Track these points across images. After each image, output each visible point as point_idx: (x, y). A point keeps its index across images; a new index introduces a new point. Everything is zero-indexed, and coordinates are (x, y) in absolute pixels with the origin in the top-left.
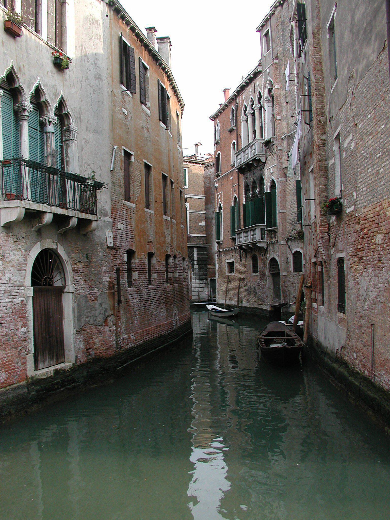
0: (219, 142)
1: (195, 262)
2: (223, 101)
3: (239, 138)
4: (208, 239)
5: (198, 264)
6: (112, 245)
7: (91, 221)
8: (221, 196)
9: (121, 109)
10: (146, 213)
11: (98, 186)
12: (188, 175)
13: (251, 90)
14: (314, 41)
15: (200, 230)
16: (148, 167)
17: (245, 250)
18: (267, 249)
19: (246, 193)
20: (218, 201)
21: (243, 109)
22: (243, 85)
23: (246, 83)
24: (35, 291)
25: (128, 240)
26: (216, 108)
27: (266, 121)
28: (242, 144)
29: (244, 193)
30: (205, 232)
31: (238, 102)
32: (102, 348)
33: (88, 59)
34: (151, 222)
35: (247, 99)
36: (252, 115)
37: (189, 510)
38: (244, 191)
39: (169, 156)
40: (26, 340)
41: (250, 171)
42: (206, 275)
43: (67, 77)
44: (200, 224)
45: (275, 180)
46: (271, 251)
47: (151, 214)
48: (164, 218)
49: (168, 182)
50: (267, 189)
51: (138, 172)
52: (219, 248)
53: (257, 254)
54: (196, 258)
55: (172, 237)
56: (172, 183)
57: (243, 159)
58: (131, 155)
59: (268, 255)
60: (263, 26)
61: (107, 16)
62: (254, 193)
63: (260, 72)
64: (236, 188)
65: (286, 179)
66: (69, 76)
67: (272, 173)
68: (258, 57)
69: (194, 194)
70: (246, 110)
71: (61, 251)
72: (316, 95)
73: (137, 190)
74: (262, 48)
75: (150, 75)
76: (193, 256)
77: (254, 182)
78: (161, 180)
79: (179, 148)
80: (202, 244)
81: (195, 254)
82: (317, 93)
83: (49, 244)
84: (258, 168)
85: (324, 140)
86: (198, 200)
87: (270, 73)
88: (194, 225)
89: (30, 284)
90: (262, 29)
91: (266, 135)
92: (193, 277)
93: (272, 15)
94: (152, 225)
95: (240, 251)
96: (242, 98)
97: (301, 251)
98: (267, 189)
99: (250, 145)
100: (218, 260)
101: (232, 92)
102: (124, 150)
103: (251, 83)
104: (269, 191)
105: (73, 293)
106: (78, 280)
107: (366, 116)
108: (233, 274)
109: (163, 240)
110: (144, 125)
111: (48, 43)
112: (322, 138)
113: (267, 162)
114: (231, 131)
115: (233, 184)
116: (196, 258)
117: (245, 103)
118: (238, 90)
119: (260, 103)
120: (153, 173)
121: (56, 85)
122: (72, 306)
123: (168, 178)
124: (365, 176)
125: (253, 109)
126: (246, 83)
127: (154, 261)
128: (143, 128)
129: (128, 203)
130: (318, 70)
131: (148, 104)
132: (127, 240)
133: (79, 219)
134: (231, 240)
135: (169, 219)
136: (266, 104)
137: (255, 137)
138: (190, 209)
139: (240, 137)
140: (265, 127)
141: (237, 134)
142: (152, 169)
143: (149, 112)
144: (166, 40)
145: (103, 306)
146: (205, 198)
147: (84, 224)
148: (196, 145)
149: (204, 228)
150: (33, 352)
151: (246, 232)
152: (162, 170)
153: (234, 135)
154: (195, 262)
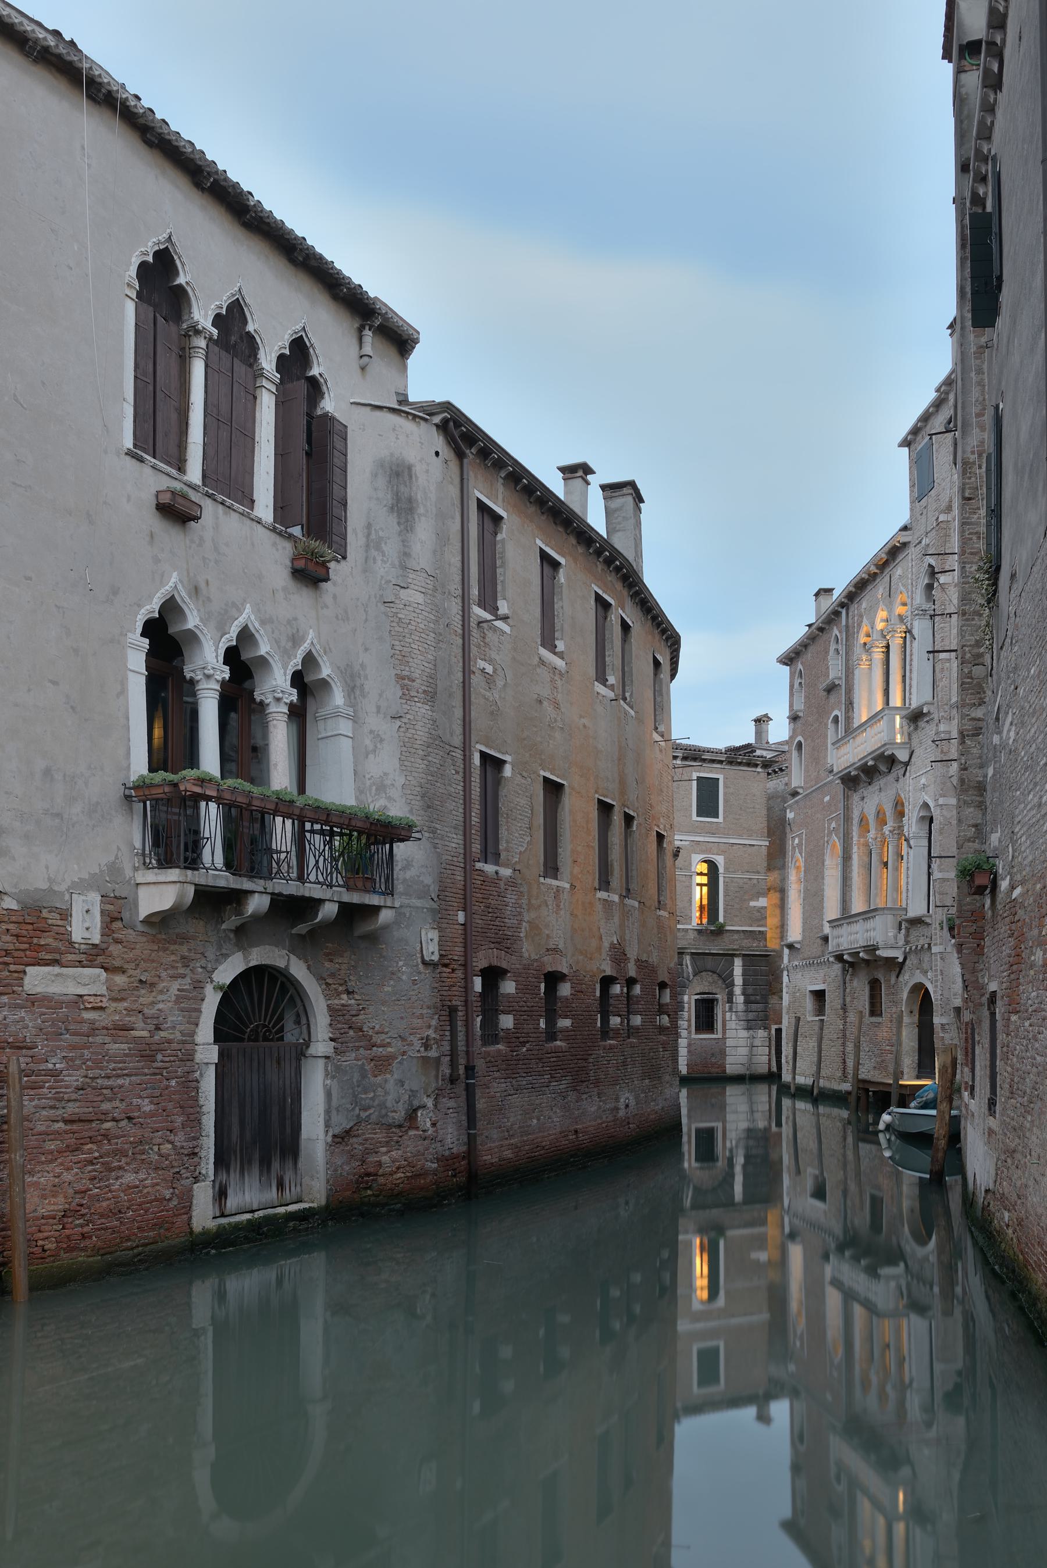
1: (738, 990)
5: (744, 994)
6: (436, 958)
7: (376, 910)
11: (385, 833)
12: (725, 794)
14: (964, 484)
16: (553, 789)
22: (862, 579)
24: (221, 1054)
33: (384, 555)
34: (558, 906)
40: (195, 1154)
42: (766, 1018)
43: (327, 598)
44: (752, 904)
45: (931, 804)
54: (738, 980)
58: (504, 762)
61: (437, 454)
66: (335, 597)
68: (903, 517)
69: (740, 836)
71: (299, 970)
76: (731, 974)
79: (659, 738)
83: (259, 956)
85: (979, 720)
86: (750, 850)
88: (736, 906)
89: (211, 1038)
94: (562, 912)
105: (327, 1057)
106: (342, 1031)
107: (1029, 671)
110: (545, 692)
111: (274, 528)
112: (973, 715)
116: (738, 980)
121: (296, 619)
122: (325, 1086)
123: (616, 809)
124: (1025, 808)
130: (972, 553)
131: (560, 646)
133: (343, 906)
135: (616, 898)
136: (916, 623)
137: (887, 703)
138: (726, 869)
140: (911, 679)
142: (567, 790)
143: (560, 663)
144: (625, 490)
145: (406, 1086)
147: (351, 914)
152: (596, 792)
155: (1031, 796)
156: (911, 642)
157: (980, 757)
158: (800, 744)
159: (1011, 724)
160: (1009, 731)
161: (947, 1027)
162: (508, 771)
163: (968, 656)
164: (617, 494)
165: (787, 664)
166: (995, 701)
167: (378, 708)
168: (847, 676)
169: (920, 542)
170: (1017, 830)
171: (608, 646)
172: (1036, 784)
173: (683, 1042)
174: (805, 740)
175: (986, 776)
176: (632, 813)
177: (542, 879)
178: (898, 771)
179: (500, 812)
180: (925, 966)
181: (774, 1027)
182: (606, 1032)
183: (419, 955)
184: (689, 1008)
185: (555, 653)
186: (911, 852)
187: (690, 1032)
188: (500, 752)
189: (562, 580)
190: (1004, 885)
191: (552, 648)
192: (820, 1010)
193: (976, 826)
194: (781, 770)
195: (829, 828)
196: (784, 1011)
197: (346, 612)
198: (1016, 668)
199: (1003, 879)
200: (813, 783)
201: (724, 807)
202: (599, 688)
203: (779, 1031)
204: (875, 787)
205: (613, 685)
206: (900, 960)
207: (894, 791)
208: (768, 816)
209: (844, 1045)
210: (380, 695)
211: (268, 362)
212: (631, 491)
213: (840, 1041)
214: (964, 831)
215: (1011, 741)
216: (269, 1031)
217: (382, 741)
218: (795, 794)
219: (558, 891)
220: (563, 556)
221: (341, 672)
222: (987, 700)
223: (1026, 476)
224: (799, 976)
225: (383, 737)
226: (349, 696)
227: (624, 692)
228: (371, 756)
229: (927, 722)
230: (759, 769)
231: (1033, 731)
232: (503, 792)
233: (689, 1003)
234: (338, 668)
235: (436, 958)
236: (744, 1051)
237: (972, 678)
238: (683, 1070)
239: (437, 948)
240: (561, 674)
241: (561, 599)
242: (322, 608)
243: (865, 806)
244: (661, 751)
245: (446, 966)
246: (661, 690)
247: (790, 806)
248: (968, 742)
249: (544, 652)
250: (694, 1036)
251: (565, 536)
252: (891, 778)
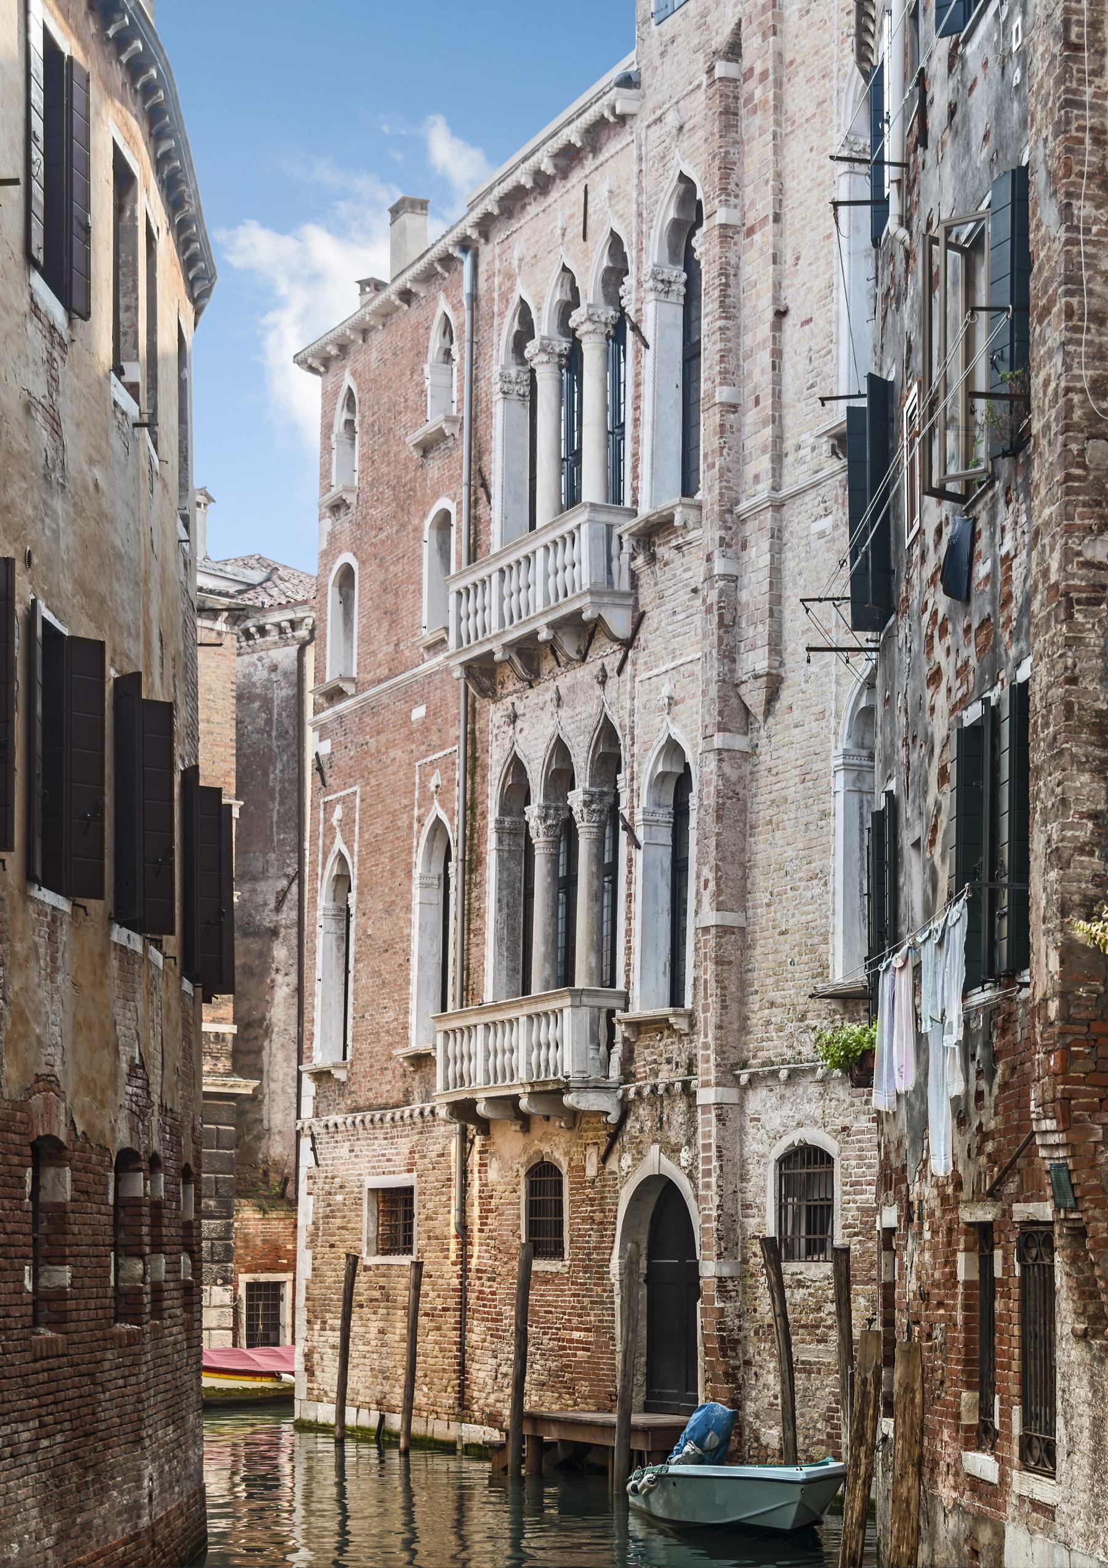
8: (349, 810)
18: (616, 1132)
34: (54, 960)
48: (115, 937)
91: (645, 484)
94: (59, 978)
97: (831, 1145)
109: (107, 1067)
112: (1089, 555)
136: (649, 309)
140: (636, 441)
156: (638, 353)
158: (347, 573)
161: (730, 1285)
163: (1077, 414)
168: (473, 419)
169: (660, 119)
174: (362, 563)
178: (605, 654)
180: (676, 1135)
186: (639, 856)
195: (424, 786)
200: (383, 671)
204: (543, 693)
206: (613, 1118)
207: (593, 709)
208: (238, 741)
209: (462, 1327)
213: (451, 1319)
214: (1072, 826)
224: (344, 1150)
229: (678, 548)
237: (1084, 466)
243: (520, 738)
248: (1079, 617)
252: (586, 673)
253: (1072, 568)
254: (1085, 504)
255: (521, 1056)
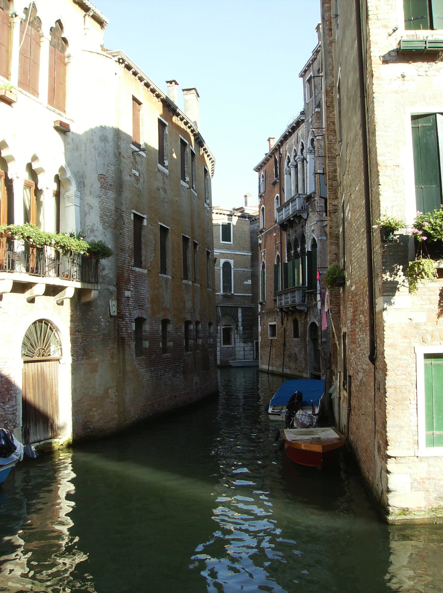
0: (263, 195)
1: (240, 324)
2: (267, 151)
3: (282, 192)
4: (254, 298)
6: (115, 314)
8: (265, 253)
9: (132, 171)
10: (160, 279)
13: (294, 141)
15: (245, 289)
16: (164, 231)
17: (287, 313)
19: (288, 252)
20: (261, 259)
21: (286, 161)
23: (289, 132)
25: (137, 308)
26: (261, 158)
27: (308, 174)
28: (285, 199)
29: (286, 251)
30: (250, 291)
31: (281, 152)
32: (102, 421)
34: (167, 287)
35: (290, 150)
36: (295, 167)
37: (206, 587)
38: (286, 249)
39: (191, 216)
41: (292, 227)
44: (245, 283)
45: (316, 239)
46: (311, 315)
47: (167, 279)
49: (190, 244)
50: (308, 248)
51: (151, 237)
52: (262, 310)
53: (298, 317)
54: (240, 319)
55: (193, 303)
56: (195, 245)
57: (284, 215)
58: (144, 218)
59: (308, 319)
60: (305, 71)
62: (296, 252)
63: (303, 121)
64: (279, 245)
65: (327, 238)
67: (313, 230)
68: (301, 107)
69: (240, 250)
70: (289, 162)
72: (329, 158)
73: (150, 254)
74: (305, 95)
75: (169, 131)
77: (296, 240)
78: (181, 243)
80: (247, 304)
81: (240, 315)
82: (330, 155)
84: (300, 225)
85: (336, 206)
86: (244, 257)
87: (313, 123)
90: (304, 75)
91: (308, 189)
92: (238, 340)
93: (314, 60)
94: (168, 290)
95: (282, 314)
96: (285, 149)
98: (308, 248)
99: (292, 200)
100: (260, 323)
101: (274, 143)
102: (134, 213)
103: (294, 132)
104: (310, 250)
107: (356, 188)
108: (276, 338)
110: (161, 185)
112: (333, 203)
113: (308, 219)
114: (274, 184)
115: (276, 241)
116: (240, 319)
117: (288, 154)
118: (282, 140)
119: (302, 154)
120: (170, 237)
123: (190, 240)
124: (356, 249)
125: (296, 161)
126: (289, 132)
127: (170, 328)
128: (159, 189)
129: (137, 269)
130: (331, 131)
132: (136, 308)
134: (273, 302)
135: (190, 283)
136: (308, 156)
139: (284, 191)
140: (306, 181)
141: (280, 188)
142: (170, 231)
143: (166, 171)
146: (251, 254)
148: (246, 196)
149: (250, 287)
150: (22, 426)
151: (286, 294)
153: (277, 188)
154: (240, 324)
155: (358, 245)
156: (306, 164)
157: (337, 223)
159: (349, 210)
160: (348, 213)
162: (145, 223)
164: (189, 93)
165: (257, 171)
166: (342, 198)
167: (91, 192)
170: (353, 259)
171: (186, 163)
172: (360, 240)
173: (218, 349)
175: (339, 231)
176: (196, 242)
177: (160, 275)
179: (142, 242)
181: (255, 341)
182: (187, 348)
183: (109, 313)
184: (220, 332)
185: (164, 166)
187: (221, 345)
188: (142, 213)
189: (167, 132)
190: (348, 283)
191: (163, 164)
192: (273, 334)
193: (336, 254)
194: (256, 220)
196: (259, 334)
197: (77, 146)
198: (350, 186)
199: (348, 281)
201: (233, 237)
202: (182, 183)
203: (257, 343)
205: (188, 181)
210: (92, 186)
211: (45, 30)
212: (195, 92)
215: (349, 218)
216: (45, 351)
217: (92, 208)
218: (261, 232)
219: (167, 280)
220: (167, 121)
221: (75, 175)
222: (338, 196)
223: (352, 101)
225: (93, 206)
226: (78, 186)
227: (193, 184)
228: (88, 215)
230: (247, 219)
231: (358, 215)
232: (143, 233)
233: (220, 330)
234: (74, 173)
235: (115, 314)
236: (242, 353)
238: (219, 362)
239: (116, 309)
240: (167, 176)
241: (167, 141)
242: (67, 144)
244: (208, 212)
245: (120, 317)
246: (207, 184)
247: (260, 238)
249: (159, 166)
250: (223, 346)
251: (168, 112)
253: (331, 206)
254: (333, 194)
255: (289, 299)
